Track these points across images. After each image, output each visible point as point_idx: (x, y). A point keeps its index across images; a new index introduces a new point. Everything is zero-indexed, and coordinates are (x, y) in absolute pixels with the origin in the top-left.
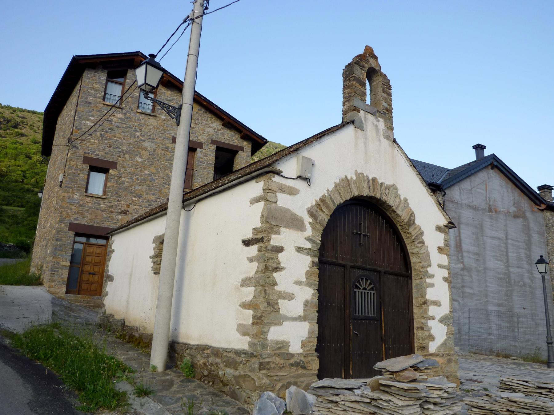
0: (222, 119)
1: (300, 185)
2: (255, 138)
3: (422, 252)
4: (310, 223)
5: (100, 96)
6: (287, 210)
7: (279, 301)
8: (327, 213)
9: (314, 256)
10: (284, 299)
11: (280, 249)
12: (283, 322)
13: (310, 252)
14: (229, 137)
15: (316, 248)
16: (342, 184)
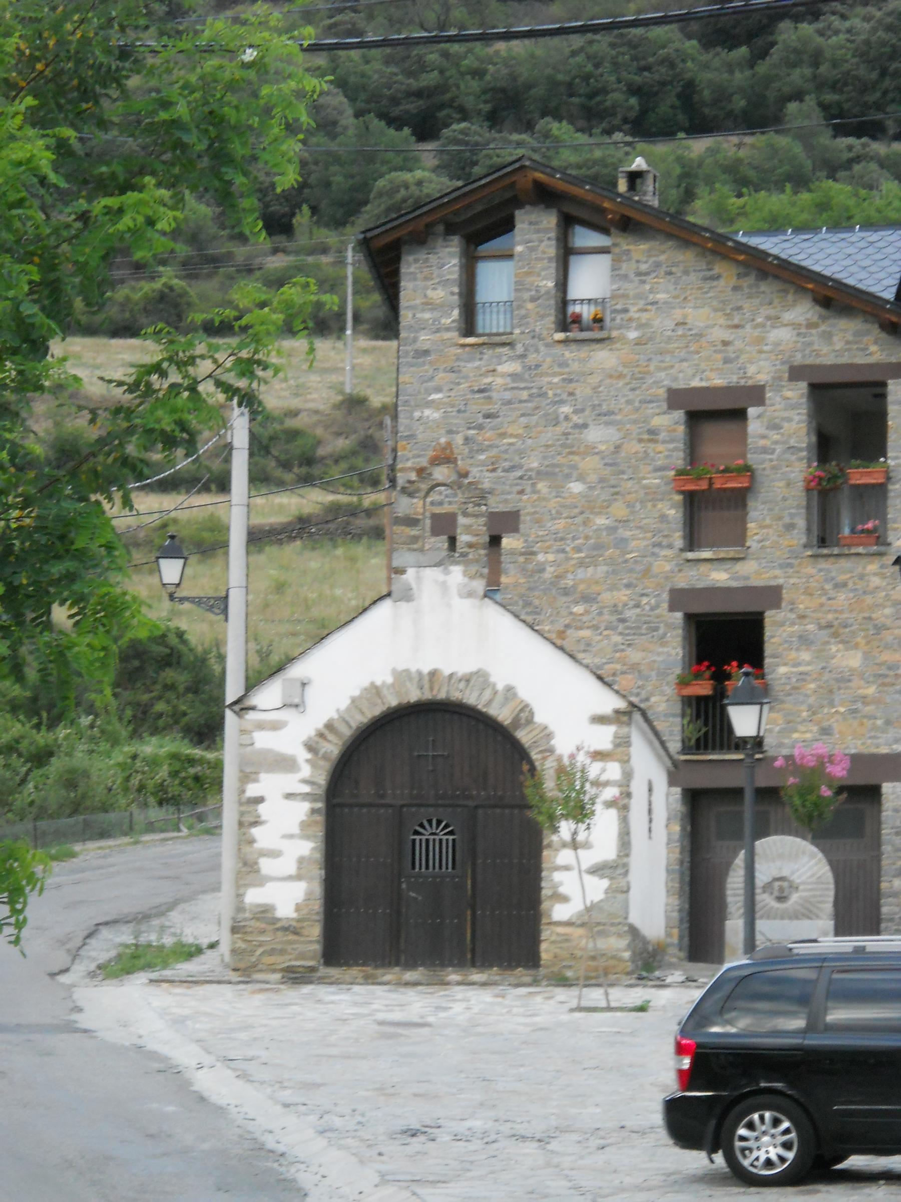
5: (449, 321)
6: (269, 751)
9: (315, 801)
11: (260, 800)
14: (848, 342)
15: (321, 791)
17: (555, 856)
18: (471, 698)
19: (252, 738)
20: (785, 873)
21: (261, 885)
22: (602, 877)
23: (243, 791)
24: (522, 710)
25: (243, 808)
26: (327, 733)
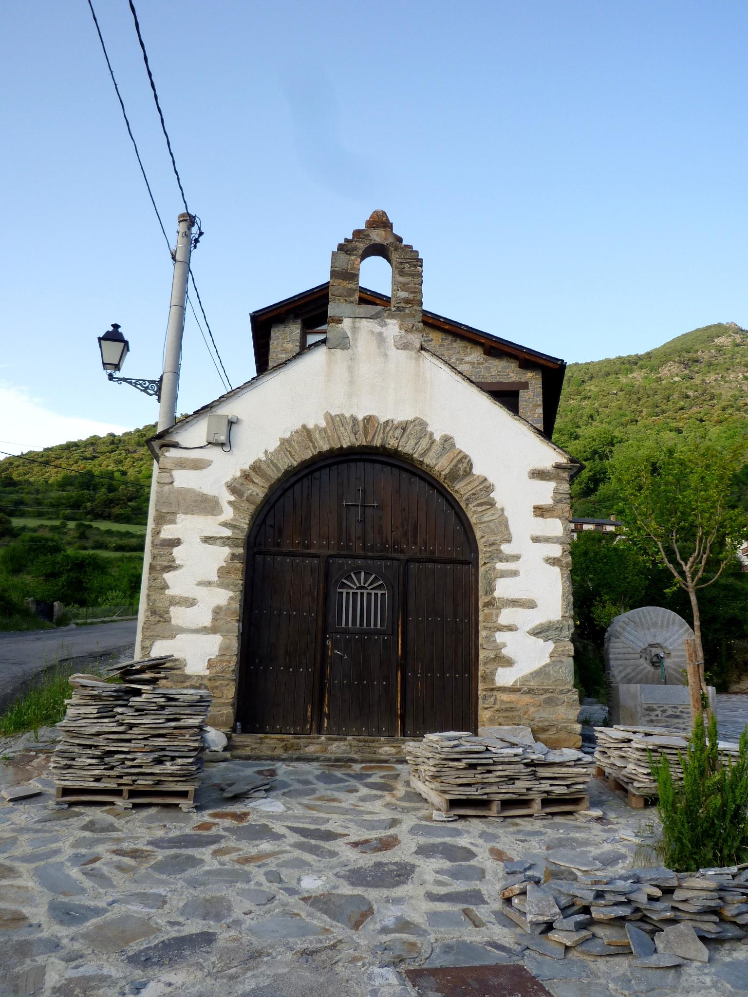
0: (481, 345)
1: (214, 454)
2: (542, 362)
3: (487, 519)
4: (230, 503)
6: (189, 491)
7: (172, 609)
8: (262, 484)
9: (236, 546)
10: (181, 606)
11: (176, 542)
12: (176, 635)
13: (230, 541)
14: (499, 372)
15: (242, 536)
16: (295, 439)
17: (497, 616)
18: (407, 446)
19: (171, 476)
20: (659, 640)
21: (173, 637)
22: (546, 640)
23: (158, 533)
24: (460, 461)
25: (156, 551)
26: (253, 474)
